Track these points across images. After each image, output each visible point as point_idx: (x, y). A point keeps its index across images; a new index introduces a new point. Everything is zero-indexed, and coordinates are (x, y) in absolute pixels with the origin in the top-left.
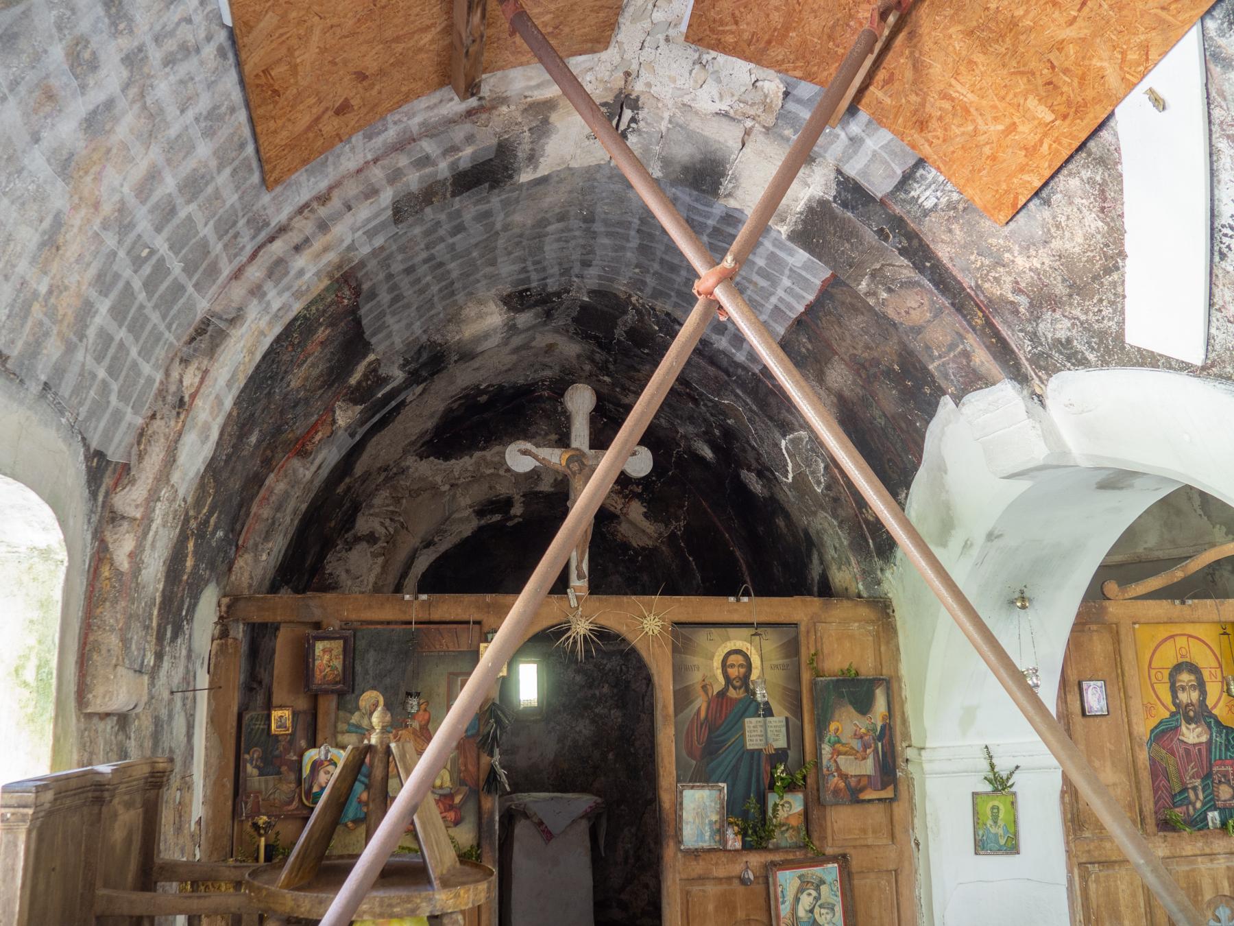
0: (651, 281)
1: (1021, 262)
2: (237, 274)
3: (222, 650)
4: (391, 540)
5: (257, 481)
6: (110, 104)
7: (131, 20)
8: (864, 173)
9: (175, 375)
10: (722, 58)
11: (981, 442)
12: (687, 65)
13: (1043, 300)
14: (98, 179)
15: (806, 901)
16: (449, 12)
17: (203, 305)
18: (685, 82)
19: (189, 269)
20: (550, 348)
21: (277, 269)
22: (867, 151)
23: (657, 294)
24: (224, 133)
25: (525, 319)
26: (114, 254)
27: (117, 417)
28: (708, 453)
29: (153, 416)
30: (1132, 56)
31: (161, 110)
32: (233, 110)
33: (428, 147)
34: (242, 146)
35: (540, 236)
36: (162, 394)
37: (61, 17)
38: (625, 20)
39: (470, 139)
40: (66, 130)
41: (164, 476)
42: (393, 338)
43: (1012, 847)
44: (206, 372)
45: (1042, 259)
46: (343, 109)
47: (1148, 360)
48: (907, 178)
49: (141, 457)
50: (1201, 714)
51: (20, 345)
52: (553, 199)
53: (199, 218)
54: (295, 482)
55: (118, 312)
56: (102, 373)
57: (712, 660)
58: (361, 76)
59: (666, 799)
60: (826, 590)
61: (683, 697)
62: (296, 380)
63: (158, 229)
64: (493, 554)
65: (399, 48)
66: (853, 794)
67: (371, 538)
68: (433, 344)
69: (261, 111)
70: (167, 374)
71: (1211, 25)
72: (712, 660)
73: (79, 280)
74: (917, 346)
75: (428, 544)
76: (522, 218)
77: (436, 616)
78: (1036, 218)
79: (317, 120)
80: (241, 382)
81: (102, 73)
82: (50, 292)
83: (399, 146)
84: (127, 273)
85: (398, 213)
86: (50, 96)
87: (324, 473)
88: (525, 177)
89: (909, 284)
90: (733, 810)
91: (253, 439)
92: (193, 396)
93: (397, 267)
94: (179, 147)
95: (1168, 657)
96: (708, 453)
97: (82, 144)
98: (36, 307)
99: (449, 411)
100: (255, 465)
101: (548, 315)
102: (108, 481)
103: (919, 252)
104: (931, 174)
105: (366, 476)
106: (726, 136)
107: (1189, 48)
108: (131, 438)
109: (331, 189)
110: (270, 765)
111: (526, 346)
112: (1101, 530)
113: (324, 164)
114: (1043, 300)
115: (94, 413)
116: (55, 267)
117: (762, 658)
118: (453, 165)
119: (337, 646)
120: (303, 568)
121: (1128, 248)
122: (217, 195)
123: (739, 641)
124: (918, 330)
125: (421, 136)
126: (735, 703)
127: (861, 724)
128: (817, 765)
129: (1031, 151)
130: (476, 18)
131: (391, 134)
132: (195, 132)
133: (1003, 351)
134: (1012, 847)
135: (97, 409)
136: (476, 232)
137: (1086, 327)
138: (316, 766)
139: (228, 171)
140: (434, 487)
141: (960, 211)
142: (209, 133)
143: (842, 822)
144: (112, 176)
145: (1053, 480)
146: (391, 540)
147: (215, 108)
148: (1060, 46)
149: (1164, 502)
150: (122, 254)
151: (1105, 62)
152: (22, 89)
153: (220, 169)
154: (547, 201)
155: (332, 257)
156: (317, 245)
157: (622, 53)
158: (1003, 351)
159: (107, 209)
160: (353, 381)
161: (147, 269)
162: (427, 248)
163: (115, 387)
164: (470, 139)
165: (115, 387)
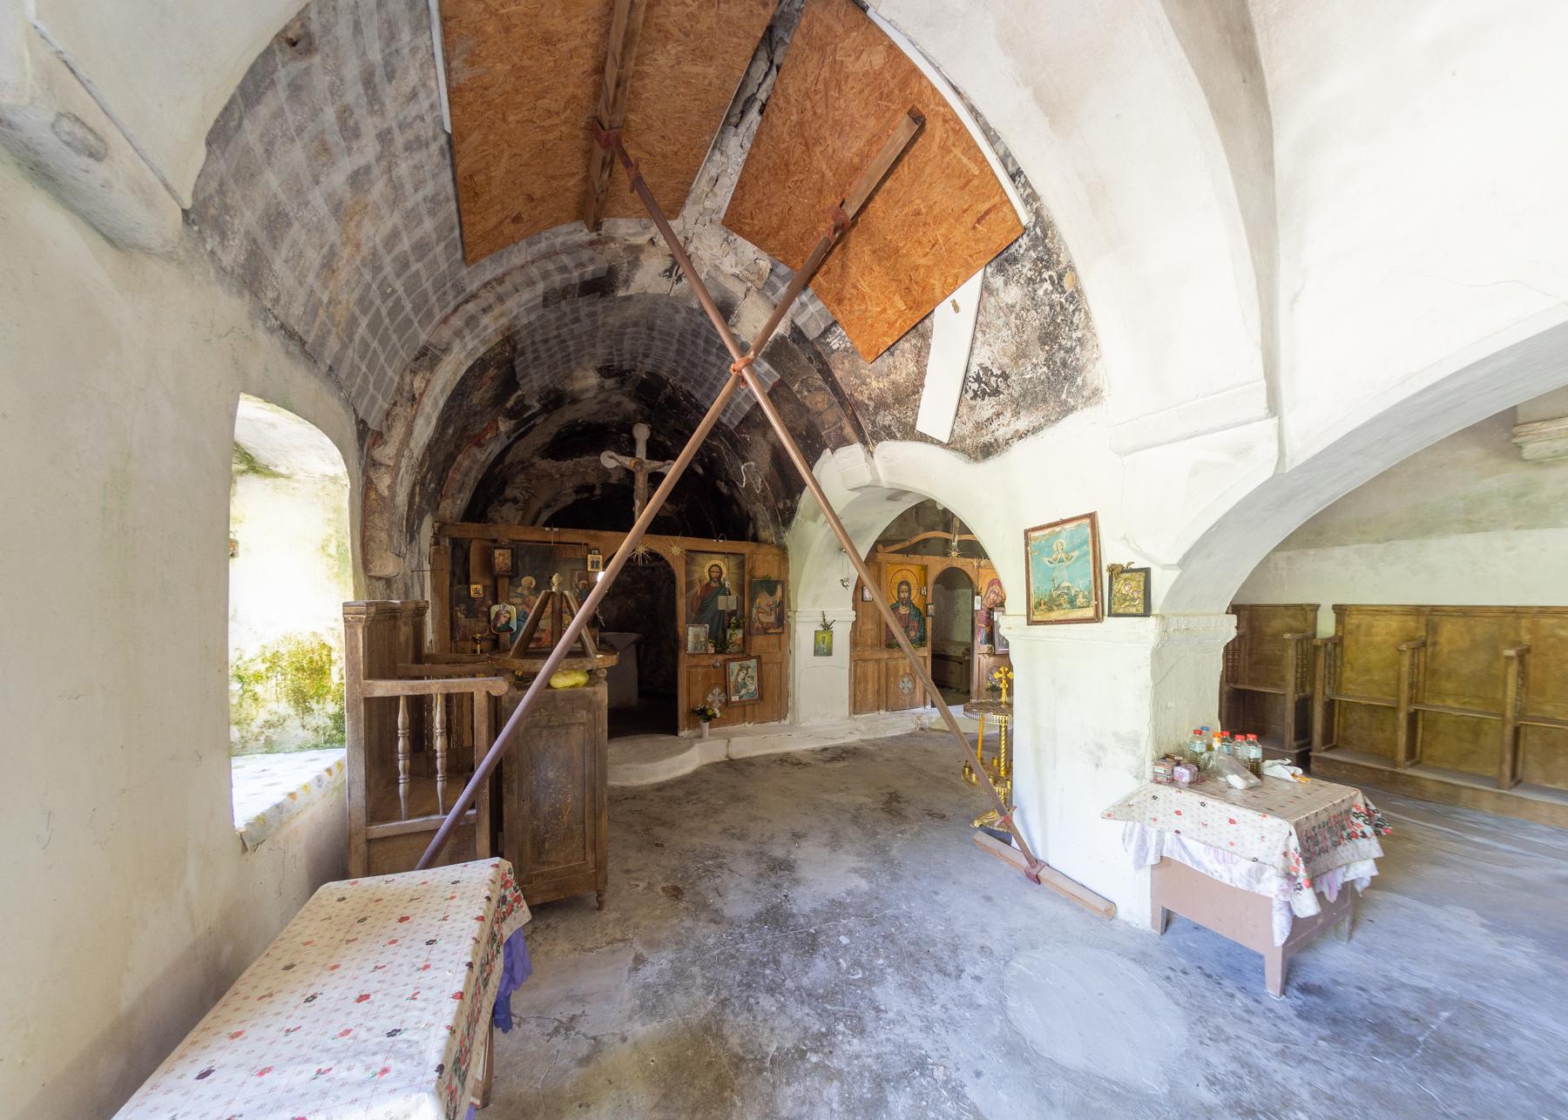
0: (681, 371)
1: (874, 384)
2: (445, 320)
3: (437, 552)
4: (527, 502)
5: (451, 458)
6: (367, 169)
7: (383, 104)
8: (805, 324)
9: (408, 379)
10: (740, 240)
11: (843, 474)
12: (720, 240)
13: (881, 405)
14: (358, 226)
15: (742, 675)
16: (588, 167)
17: (423, 337)
18: (717, 251)
19: (416, 309)
20: (619, 404)
21: (471, 321)
22: (810, 313)
23: (684, 380)
24: (441, 215)
25: (609, 383)
26: (369, 286)
27: (373, 400)
28: (700, 471)
29: (395, 404)
30: (950, 280)
31: (402, 186)
32: (448, 200)
33: (566, 260)
34: (452, 229)
35: (623, 334)
36: (399, 390)
37: (332, 84)
38: (689, 202)
39: (592, 260)
40: (337, 179)
41: (405, 442)
42: (533, 383)
43: (829, 653)
44: (428, 381)
45: (884, 384)
46: (517, 219)
47: (924, 438)
48: (827, 331)
49: (389, 429)
50: (908, 603)
51: (313, 334)
52: (633, 311)
53: (423, 273)
54: (473, 462)
55: (373, 327)
56: (364, 368)
57: (704, 568)
58: (530, 198)
59: (681, 631)
60: (755, 539)
61: (689, 585)
62: (476, 398)
63: (398, 276)
64: (607, 508)
65: (555, 184)
66: (765, 630)
67: (515, 501)
68: (557, 390)
69: (466, 206)
70: (402, 378)
71: (989, 270)
72: (704, 568)
73: (349, 298)
74: (818, 422)
75: (548, 506)
76: (613, 320)
77: (563, 539)
78: (887, 360)
79: (501, 222)
80: (448, 392)
81: (364, 142)
82: (330, 302)
83: (550, 255)
84: (378, 302)
85: (547, 300)
86: (325, 149)
87: (492, 458)
88: (621, 293)
89: (820, 389)
90: (712, 636)
91: (450, 431)
92: (421, 395)
93: (538, 338)
94: (412, 218)
95: (898, 578)
96: (700, 471)
97: (348, 195)
98: (321, 311)
99: (559, 433)
100: (451, 447)
101: (622, 383)
102: (369, 441)
103: (826, 373)
104: (839, 330)
105: (511, 464)
106: (737, 289)
107: (976, 281)
108: (381, 416)
109: (504, 275)
110: (470, 613)
111: (606, 401)
112: (883, 518)
113: (501, 257)
114: (881, 405)
115: (360, 394)
116: (332, 285)
117: (726, 567)
118: (582, 275)
119: (508, 553)
120: (477, 511)
121: (927, 382)
122: (435, 261)
123: (717, 560)
124: (820, 414)
125: (562, 252)
126: (714, 588)
127: (770, 600)
128: (750, 617)
129: (891, 325)
130: (606, 176)
131: (543, 246)
132: (423, 209)
133: (858, 428)
134: (829, 653)
135: (362, 392)
136: (586, 324)
137: (899, 420)
138: (498, 615)
139: (443, 244)
140: (550, 475)
141: (850, 352)
142: (432, 213)
143: (759, 642)
144: (368, 228)
145: (870, 492)
146: (527, 502)
147: (437, 194)
148: (917, 268)
149: (916, 507)
150: (374, 287)
151: (936, 282)
152: (306, 135)
153: (438, 241)
154: (630, 312)
155: (504, 321)
156: (497, 311)
157: (685, 224)
158: (858, 428)
159: (365, 251)
160: (509, 405)
161: (390, 303)
162: (558, 328)
163: (372, 379)
164: (592, 260)
165: (372, 379)
